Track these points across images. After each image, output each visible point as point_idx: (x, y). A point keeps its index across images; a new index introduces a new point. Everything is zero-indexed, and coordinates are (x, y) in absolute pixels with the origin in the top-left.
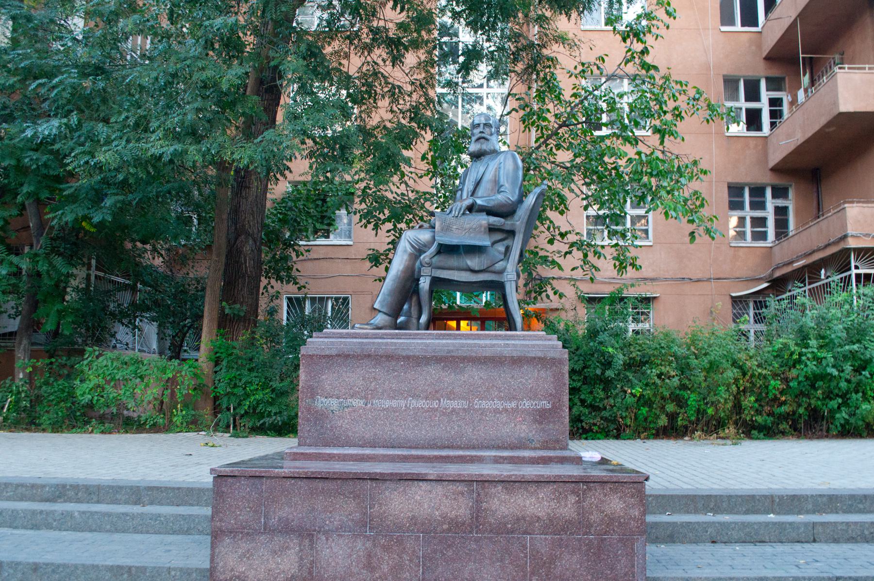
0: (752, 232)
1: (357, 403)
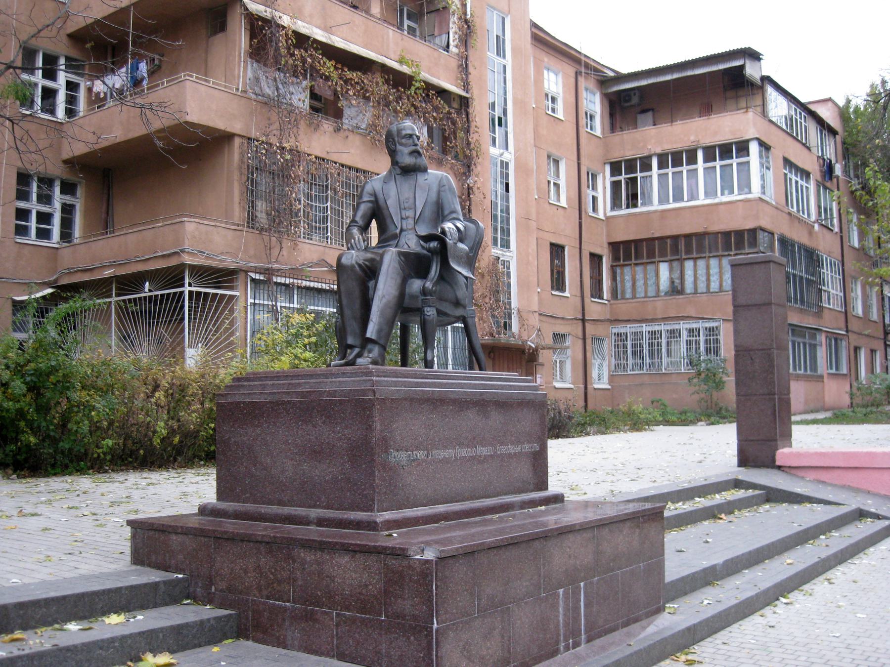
0: (37, 228)
1: (421, 454)
